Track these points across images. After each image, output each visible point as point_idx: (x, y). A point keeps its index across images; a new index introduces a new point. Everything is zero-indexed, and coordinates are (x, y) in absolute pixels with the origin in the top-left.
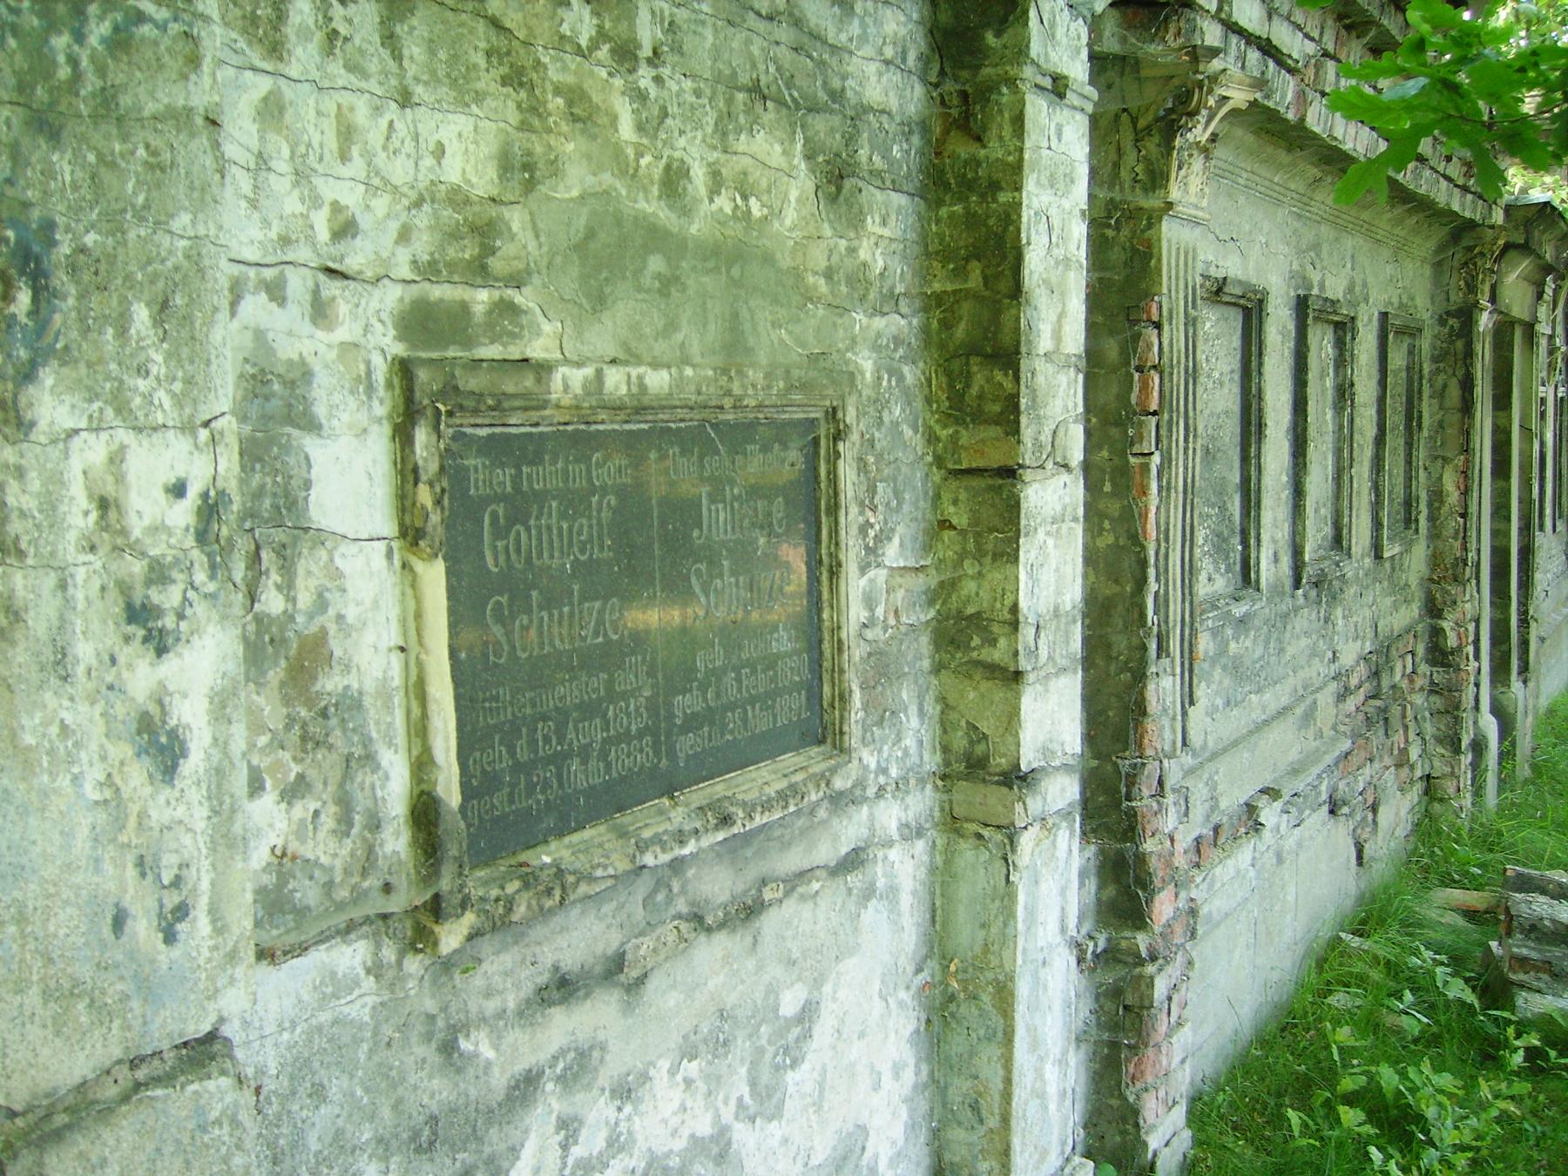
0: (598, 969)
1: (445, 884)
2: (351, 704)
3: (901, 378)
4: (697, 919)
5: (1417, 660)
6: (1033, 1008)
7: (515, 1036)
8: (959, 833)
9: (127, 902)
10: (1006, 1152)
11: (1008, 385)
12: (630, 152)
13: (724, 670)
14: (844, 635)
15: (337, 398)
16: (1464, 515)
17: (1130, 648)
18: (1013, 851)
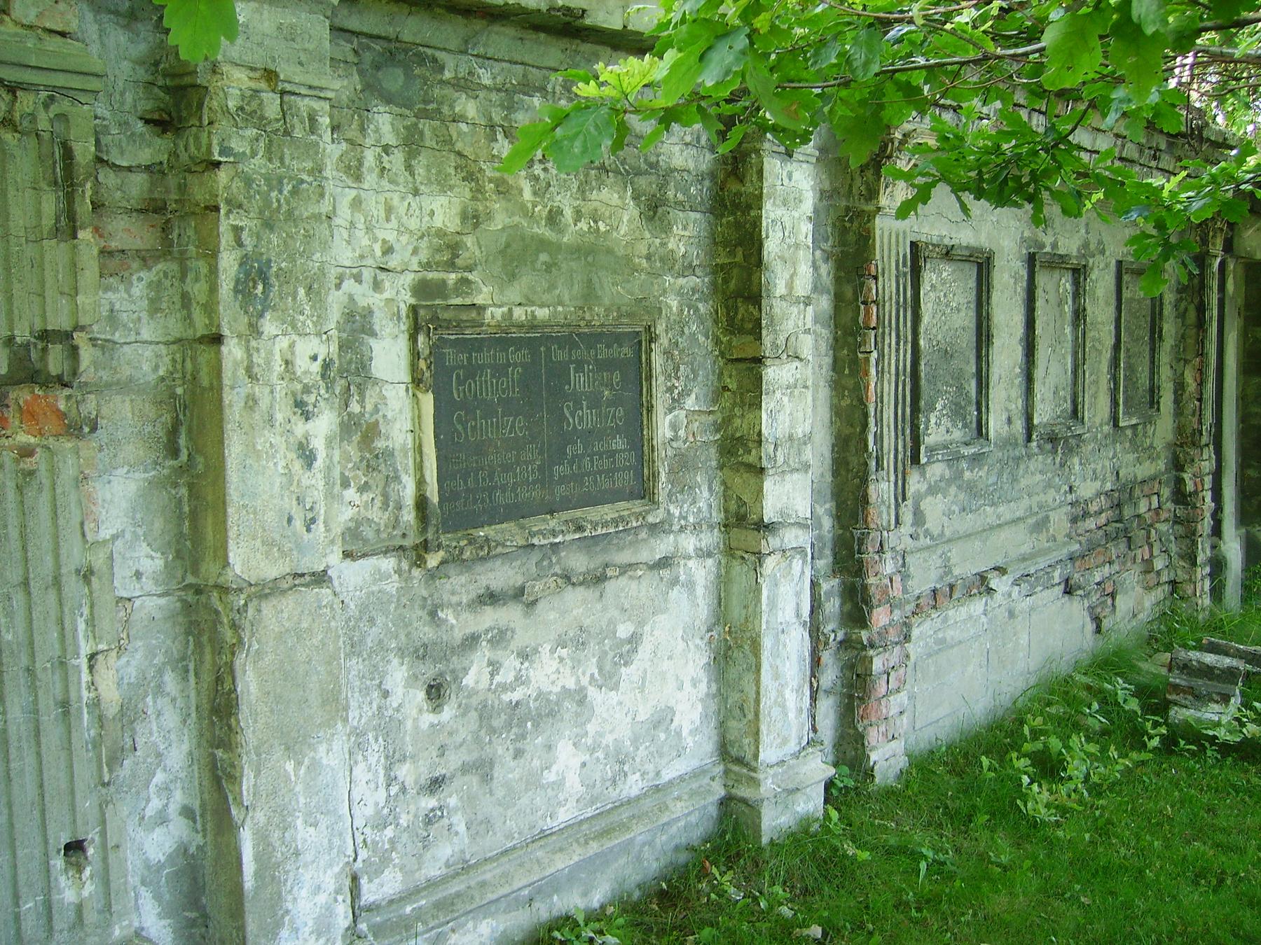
0: (511, 592)
1: (430, 535)
2: (389, 454)
3: (697, 310)
4: (567, 578)
5: (1163, 499)
6: (776, 654)
7: (466, 615)
8: (733, 556)
9: (293, 513)
10: (757, 733)
11: (756, 313)
12: (530, 205)
13: (583, 456)
14: (655, 443)
15: (384, 322)
16: (1200, 400)
17: (859, 464)
18: (761, 566)
